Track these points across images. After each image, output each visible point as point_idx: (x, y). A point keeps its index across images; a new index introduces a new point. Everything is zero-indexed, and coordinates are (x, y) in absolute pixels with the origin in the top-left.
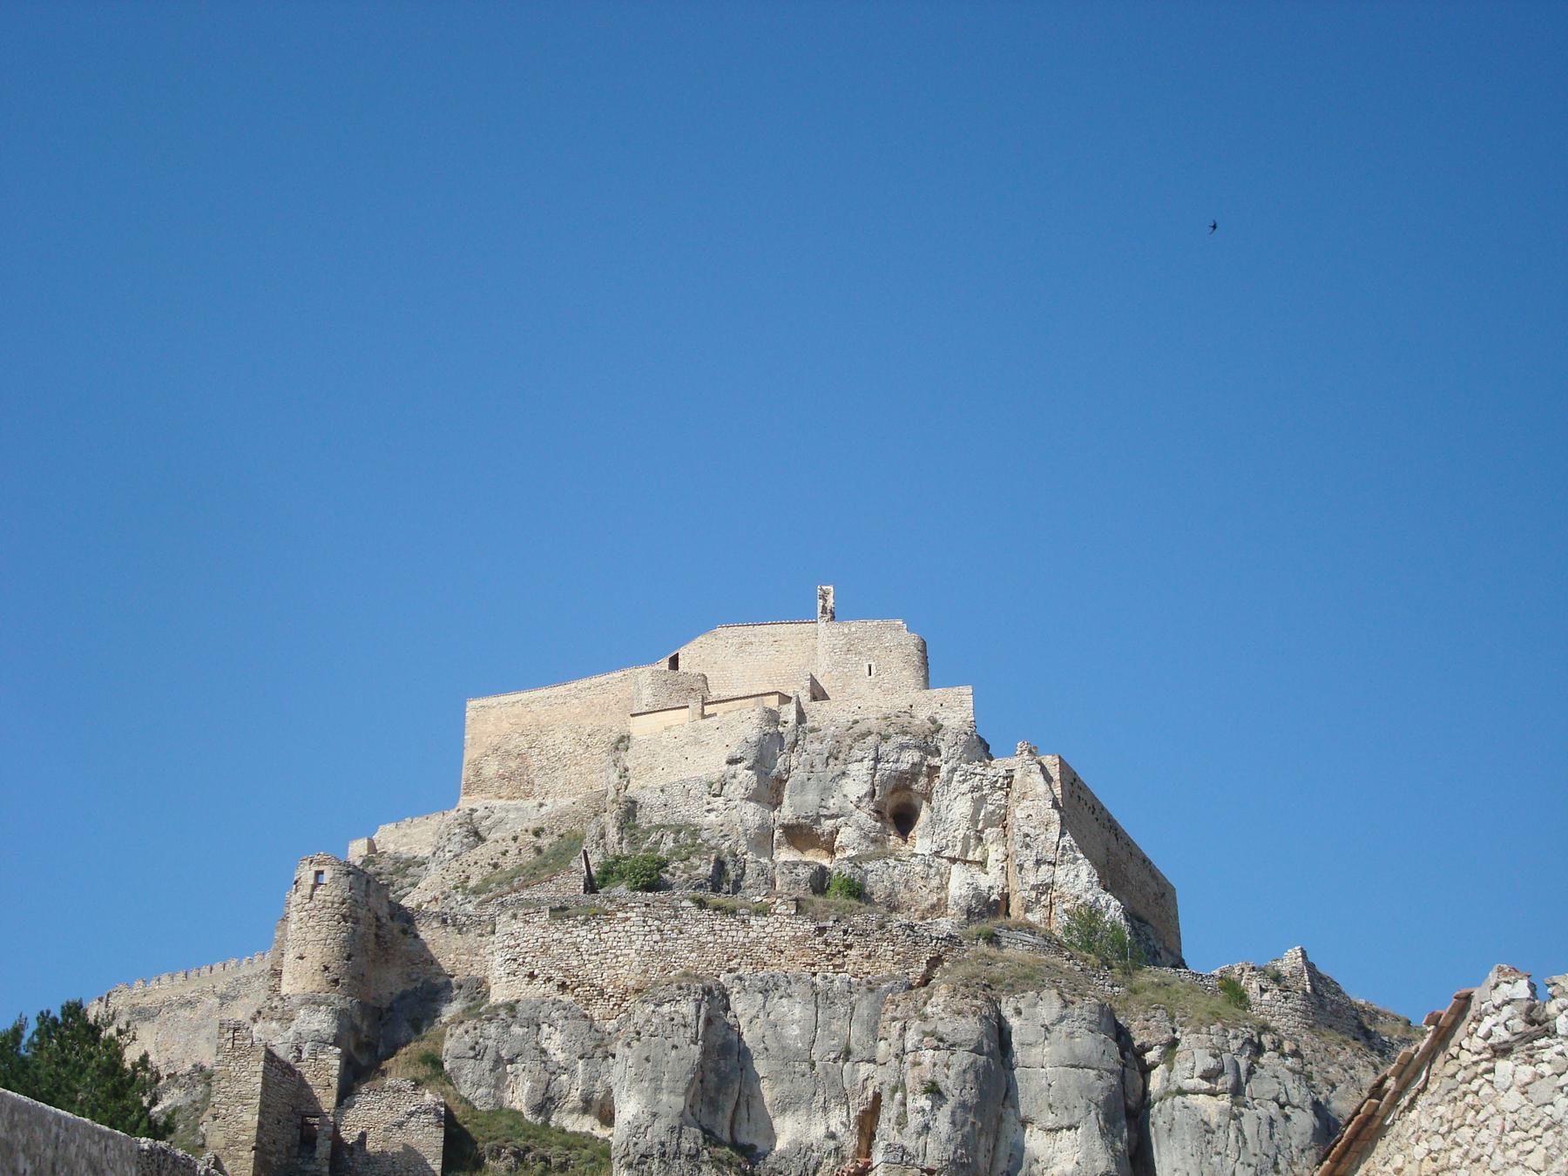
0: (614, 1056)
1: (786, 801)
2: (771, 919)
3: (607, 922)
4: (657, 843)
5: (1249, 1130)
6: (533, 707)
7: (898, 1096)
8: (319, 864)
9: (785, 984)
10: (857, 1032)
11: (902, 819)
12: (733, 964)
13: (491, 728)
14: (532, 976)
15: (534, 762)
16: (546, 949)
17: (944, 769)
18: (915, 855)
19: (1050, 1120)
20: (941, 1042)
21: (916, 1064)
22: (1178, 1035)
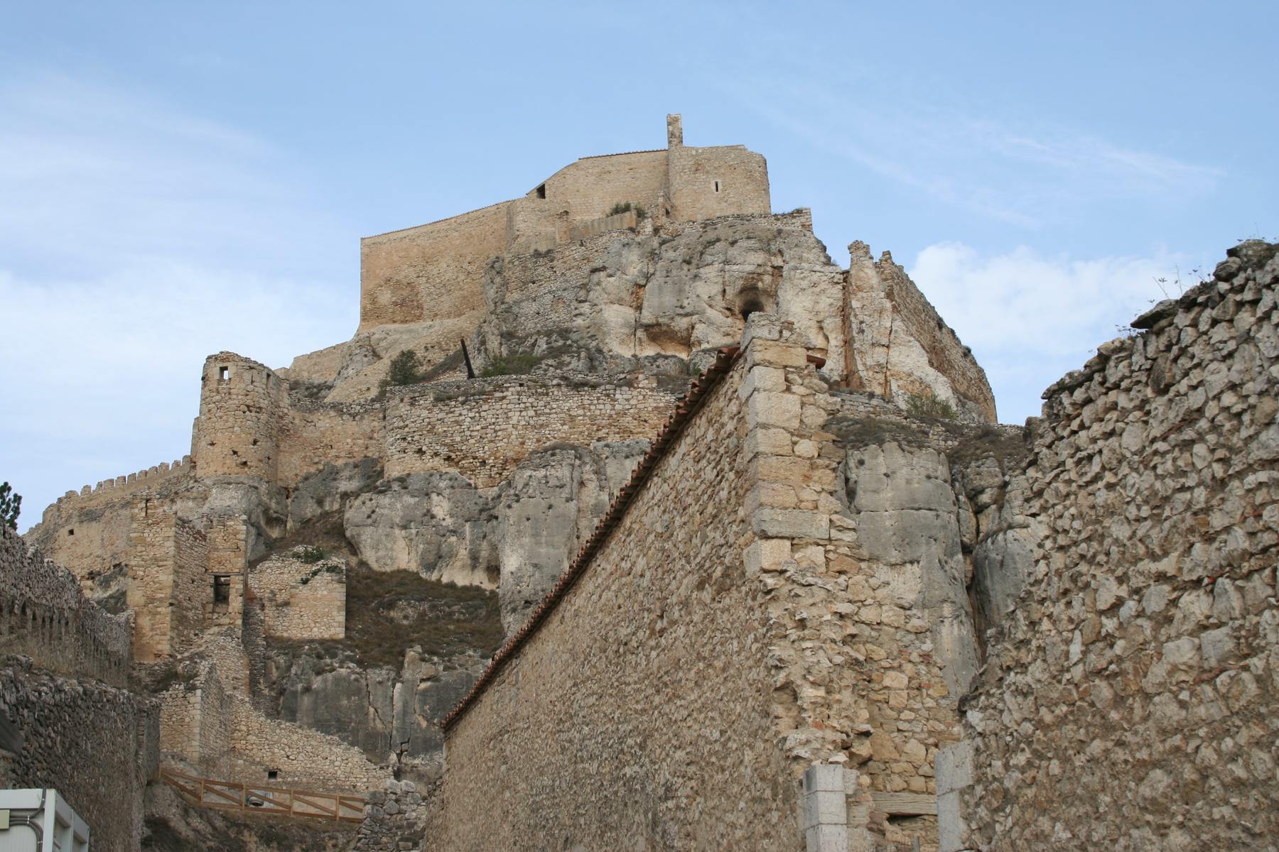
0: (496, 518)
2: (635, 393)
3: (485, 401)
4: (534, 345)
12: (601, 434)
15: (423, 288)
19: (895, 556)
22: (1007, 478)
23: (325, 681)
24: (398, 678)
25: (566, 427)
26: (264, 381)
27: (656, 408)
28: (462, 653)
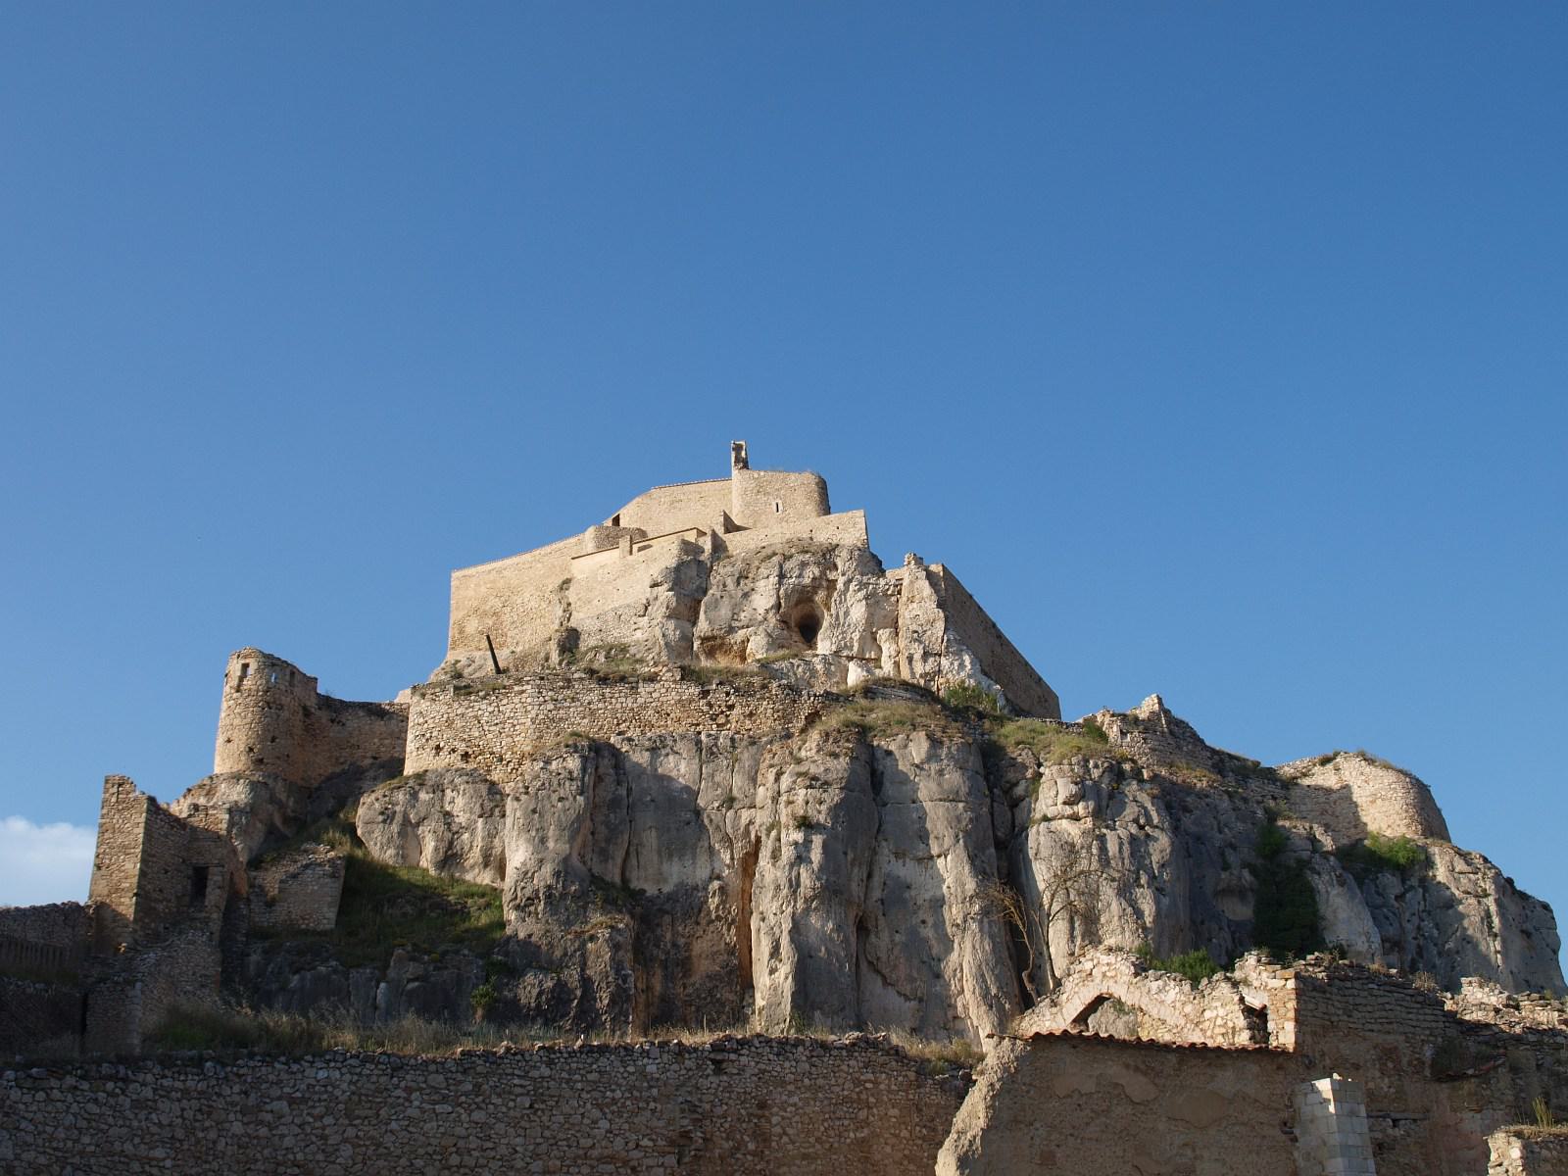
1: (702, 616)
2: (658, 686)
5: (1112, 847)
6: (505, 573)
7: (774, 833)
8: (245, 657)
9: (670, 743)
10: (738, 782)
11: (808, 629)
12: (623, 727)
13: (471, 593)
14: (438, 748)
15: (507, 619)
16: (450, 723)
17: (841, 581)
18: (817, 655)
20: (813, 781)
21: (789, 803)
23: (302, 979)
24: (383, 978)
25: (586, 721)
26: (288, 677)
27: (680, 701)
28: (457, 952)
